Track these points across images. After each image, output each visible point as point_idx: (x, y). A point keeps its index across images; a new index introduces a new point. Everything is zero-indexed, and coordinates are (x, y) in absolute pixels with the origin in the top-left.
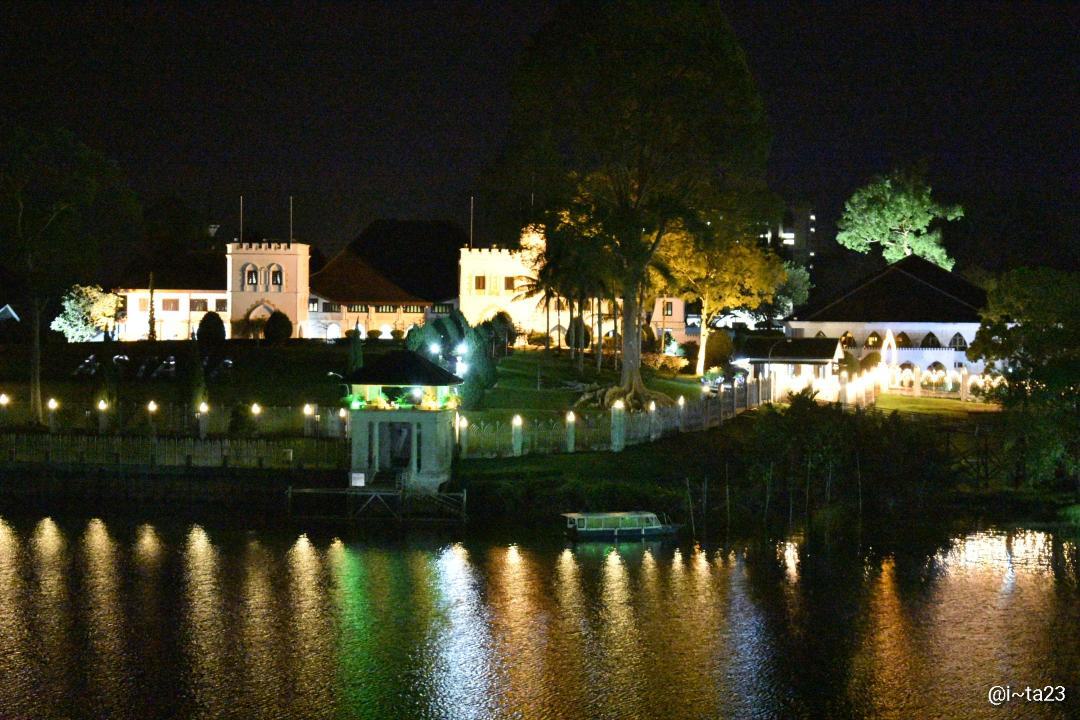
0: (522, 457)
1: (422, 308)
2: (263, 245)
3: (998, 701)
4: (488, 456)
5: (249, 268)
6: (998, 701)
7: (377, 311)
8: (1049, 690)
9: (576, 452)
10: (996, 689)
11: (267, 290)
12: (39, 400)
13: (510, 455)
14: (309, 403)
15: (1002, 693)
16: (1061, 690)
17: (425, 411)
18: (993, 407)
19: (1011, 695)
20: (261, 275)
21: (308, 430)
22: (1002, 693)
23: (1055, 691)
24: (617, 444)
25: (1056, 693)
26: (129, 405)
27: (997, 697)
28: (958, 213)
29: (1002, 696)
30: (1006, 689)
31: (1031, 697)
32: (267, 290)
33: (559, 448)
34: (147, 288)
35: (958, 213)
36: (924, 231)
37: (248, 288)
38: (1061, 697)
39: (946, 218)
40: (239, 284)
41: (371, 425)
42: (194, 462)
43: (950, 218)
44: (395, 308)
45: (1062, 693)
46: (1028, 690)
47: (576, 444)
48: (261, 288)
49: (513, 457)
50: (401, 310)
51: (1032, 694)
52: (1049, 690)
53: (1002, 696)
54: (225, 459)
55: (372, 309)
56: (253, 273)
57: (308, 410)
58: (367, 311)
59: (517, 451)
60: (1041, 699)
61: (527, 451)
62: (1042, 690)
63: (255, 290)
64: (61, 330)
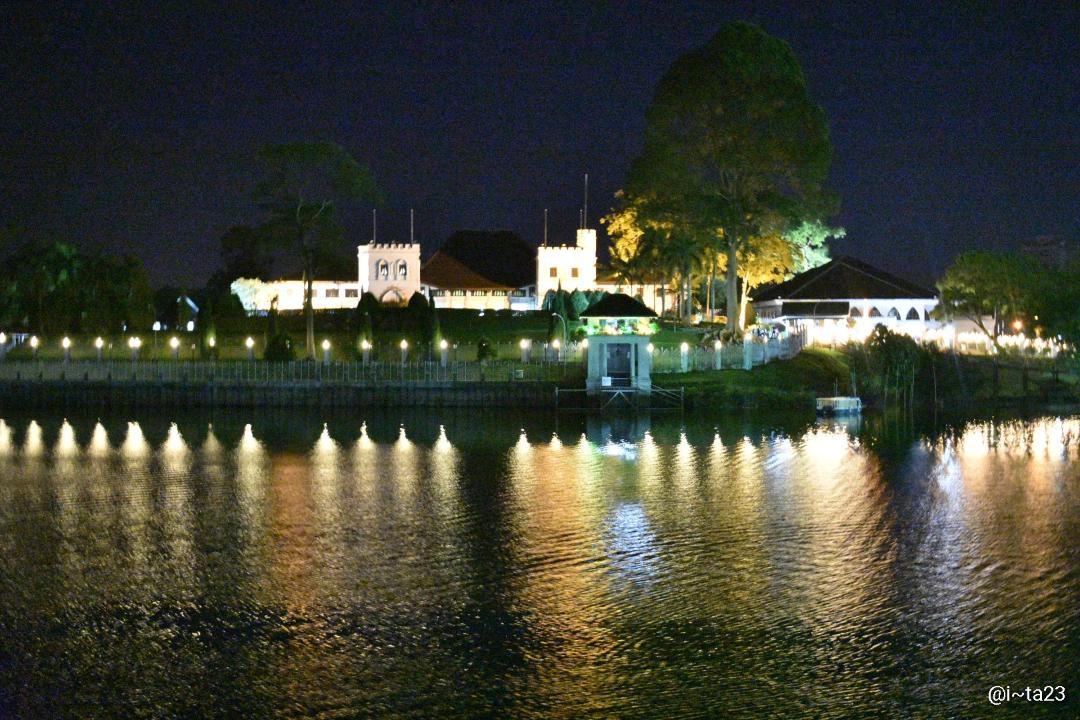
0: (688, 372)
1: (506, 292)
2: (393, 246)
3: (998, 701)
4: (666, 371)
5: (382, 263)
6: (998, 701)
7: (472, 295)
8: (1049, 690)
9: (722, 370)
10: (992, 693)
11: (395, 278)
12: (313, 346)
13: (680, 371)
14: (526, 338)
15: (1002, 693)
16: (1060, 690)
17: (641, 336)
18: (821, 403)
19: (1011, 695)
20: (391, 268)
21: (524, 359)
22: (1002, 693)
23: (1055, 691)
24: (748, 366)
25: (1056, 693)
26: (348, 348)
27: (997, 697)
28: (841, 234)
29: (1002, 696)
30: (1005, 688)
31: (1031, 697)
32: (395, 278)
33: (710, 369)
34: (299, 279)
35: (841, 234)
36: (820, 245)
37: (381, 278)
38: (1061, 697)
39: (833, 236)
40: (375, 274)
41: (601, 346)
42: (458, 379)
43: (836, 236)
44: (486, 292)
45: (1062, 693)
46: (1028, 690)
47: (722, 364)
48: (391, 277)
49: (682, 373)
50: (490, 294)
51: (1032, 694)
52: (1049, 690)
53: (1002, 696)
54: (483, 376)
55: (469, 293)
56: (385, 266)
57: (525, 344)
58: (465, 295)
59: (685, 367)
60: (1041, 699)
61: (690, 369)
62: (1042, 690)
63: (386, 279)
64: (423, 285)
